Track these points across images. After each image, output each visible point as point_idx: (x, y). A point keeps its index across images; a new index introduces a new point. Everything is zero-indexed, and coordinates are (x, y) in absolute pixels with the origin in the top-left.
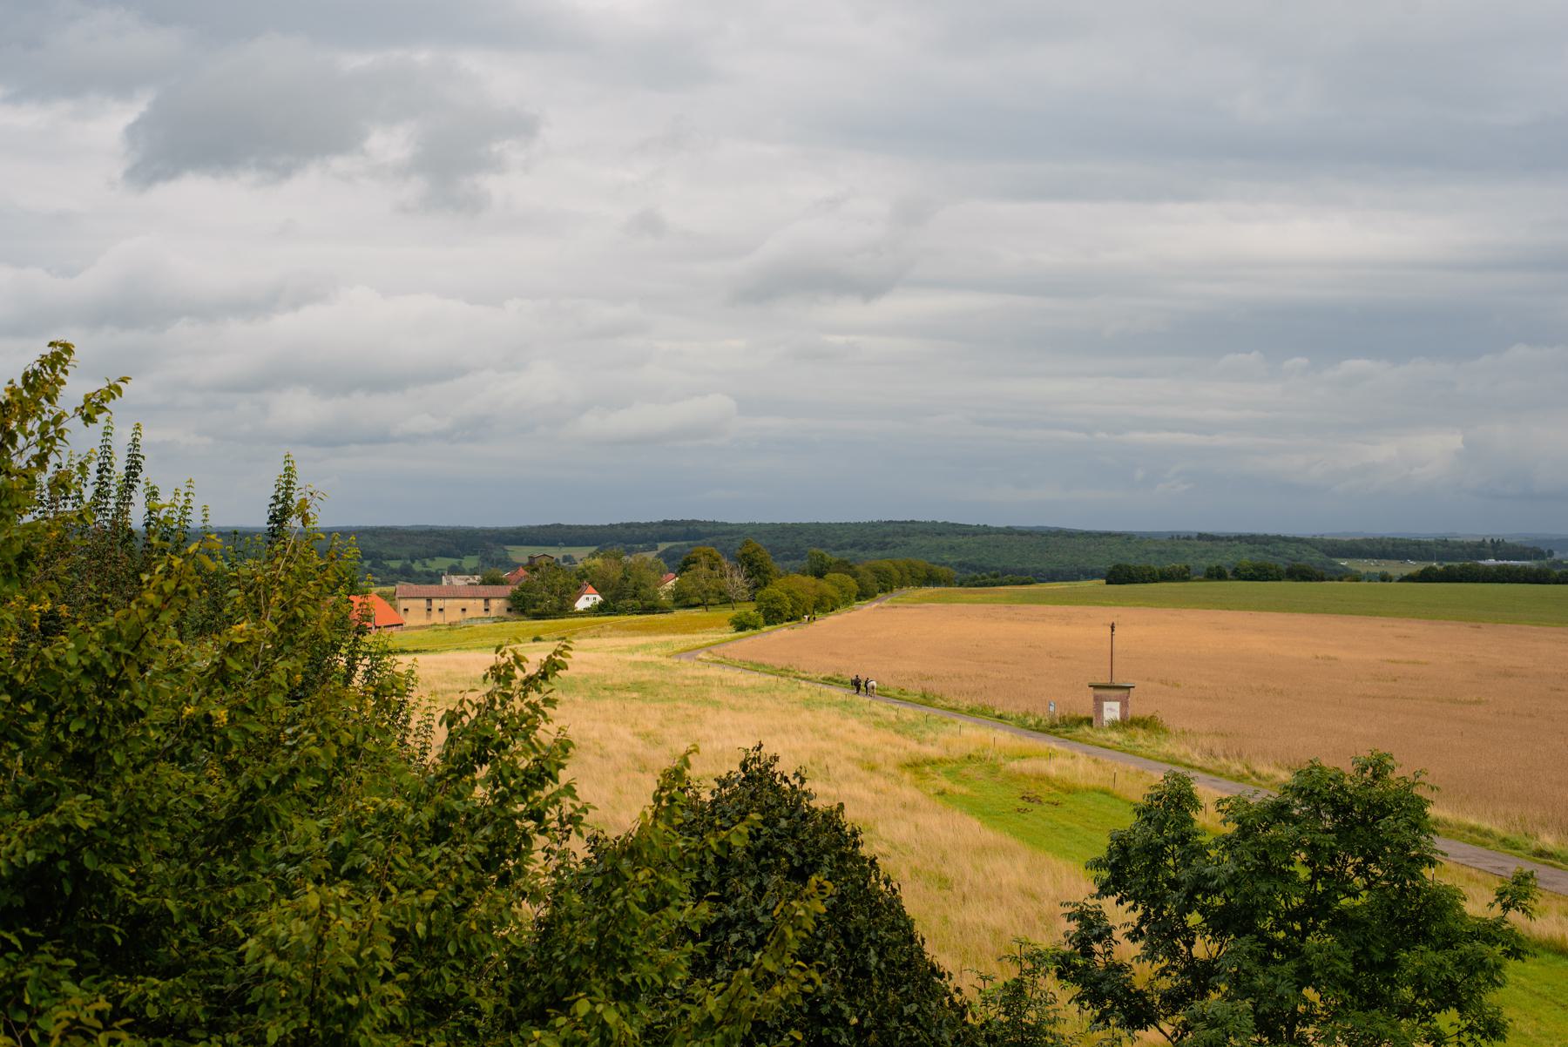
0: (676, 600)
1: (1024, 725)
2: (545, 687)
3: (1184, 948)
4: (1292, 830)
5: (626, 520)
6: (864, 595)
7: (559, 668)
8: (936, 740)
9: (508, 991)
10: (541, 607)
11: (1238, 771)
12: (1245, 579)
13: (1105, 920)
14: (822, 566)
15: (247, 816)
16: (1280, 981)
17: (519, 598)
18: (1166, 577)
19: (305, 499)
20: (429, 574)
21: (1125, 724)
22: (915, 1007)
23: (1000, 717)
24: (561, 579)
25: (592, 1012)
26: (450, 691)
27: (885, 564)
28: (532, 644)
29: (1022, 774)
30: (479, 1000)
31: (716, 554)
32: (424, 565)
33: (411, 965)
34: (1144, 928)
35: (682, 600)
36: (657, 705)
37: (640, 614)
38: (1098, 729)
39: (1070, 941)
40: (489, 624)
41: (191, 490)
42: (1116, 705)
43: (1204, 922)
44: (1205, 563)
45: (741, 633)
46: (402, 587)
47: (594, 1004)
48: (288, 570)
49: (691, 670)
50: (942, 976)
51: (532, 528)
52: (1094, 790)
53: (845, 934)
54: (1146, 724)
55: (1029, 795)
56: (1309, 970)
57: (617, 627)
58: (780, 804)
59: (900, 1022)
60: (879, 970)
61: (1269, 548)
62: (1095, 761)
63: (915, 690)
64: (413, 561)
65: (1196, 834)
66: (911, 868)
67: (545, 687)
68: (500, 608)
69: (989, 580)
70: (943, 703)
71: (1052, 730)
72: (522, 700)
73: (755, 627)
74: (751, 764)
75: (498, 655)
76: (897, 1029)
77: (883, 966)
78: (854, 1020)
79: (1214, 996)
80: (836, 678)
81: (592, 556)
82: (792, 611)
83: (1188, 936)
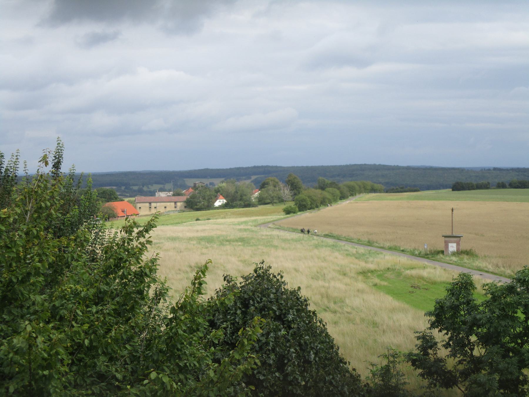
0: (259, 201)
1: (412, 254)
2: (147, 236)
3: (469, 351)
4: (516, 298)
5: (238, 166)
6: (343, 197)
7: (153, 227)
8: (373, 261)
9: (130, 369)
10: (199, 205)
11: (509, 273)
12: (515, 188)
13: (434, 339)
14: (324, 185)
15: (8, 293)
16: (510, 365)
17: (190, 202)
18: (479, 187)
19: (46, 155)
20: (150, 192)
21: (459, 253)
22: (331, 377)
23: (403, 251)
24: (208, 193)
25: (157, 378)
26: (158, 243)
27: (352, 183)
28: (195, 222)
29: (411, 276)
30: (116, 373)
31: (277, 180)
32: (148, 188)
33: (83, 358)
34: (451, 343)
35: (262, 201)
36: (249, 248)
37: (243, 207)
38: (446, 256)
39: (418, 349)
40: (177, 213)
41: (19, 154)
42: (454, 245)
43: (478, 339)
44: (497, 181)
45: (288, 215)
46: (138, 198)
47: (158, 374)
48: (39, 186)
49: (265, 232)
50: (345, 363)
51: (195, 170)
52: (444, 283)
53: (300, 345)
54: (468, 253)
55: (415, 285)
56: (524, 360)
57: (233, 214)
58: (272, 288)
59: (325, 384)
60: (316, 361)
61: (525, 174)
62: (445, 270)
63: (365, 239)
64: (143, 186)
65: (474, 300)
66: (361, 318)
67: (147, 236)
68: (181, 206)
69: (400, 190)
70: (377, 245)
71: (426, 256)
72: (137, 242)
73: (294, 213)
74: (259, 270)
75: (127, 222)
76: (323, 387)
77: (317, 359)
78: (303, 383)
79: (483, 372)
80: (330, 234)
81: (222, 182)
82: (311, 205)
83: (471, 346)
